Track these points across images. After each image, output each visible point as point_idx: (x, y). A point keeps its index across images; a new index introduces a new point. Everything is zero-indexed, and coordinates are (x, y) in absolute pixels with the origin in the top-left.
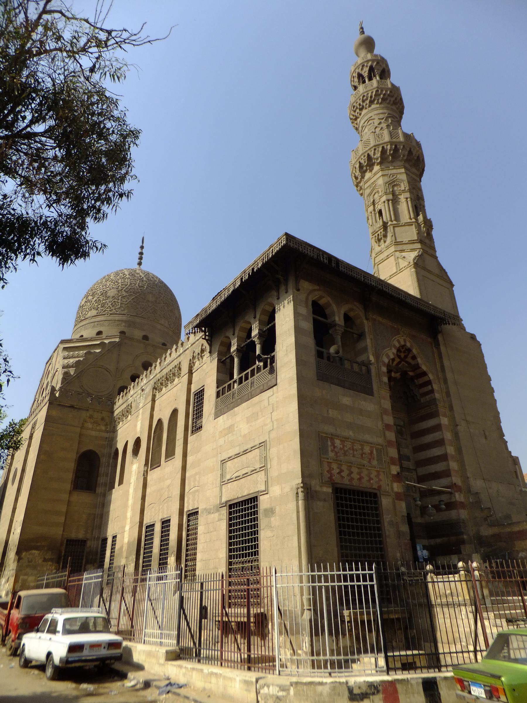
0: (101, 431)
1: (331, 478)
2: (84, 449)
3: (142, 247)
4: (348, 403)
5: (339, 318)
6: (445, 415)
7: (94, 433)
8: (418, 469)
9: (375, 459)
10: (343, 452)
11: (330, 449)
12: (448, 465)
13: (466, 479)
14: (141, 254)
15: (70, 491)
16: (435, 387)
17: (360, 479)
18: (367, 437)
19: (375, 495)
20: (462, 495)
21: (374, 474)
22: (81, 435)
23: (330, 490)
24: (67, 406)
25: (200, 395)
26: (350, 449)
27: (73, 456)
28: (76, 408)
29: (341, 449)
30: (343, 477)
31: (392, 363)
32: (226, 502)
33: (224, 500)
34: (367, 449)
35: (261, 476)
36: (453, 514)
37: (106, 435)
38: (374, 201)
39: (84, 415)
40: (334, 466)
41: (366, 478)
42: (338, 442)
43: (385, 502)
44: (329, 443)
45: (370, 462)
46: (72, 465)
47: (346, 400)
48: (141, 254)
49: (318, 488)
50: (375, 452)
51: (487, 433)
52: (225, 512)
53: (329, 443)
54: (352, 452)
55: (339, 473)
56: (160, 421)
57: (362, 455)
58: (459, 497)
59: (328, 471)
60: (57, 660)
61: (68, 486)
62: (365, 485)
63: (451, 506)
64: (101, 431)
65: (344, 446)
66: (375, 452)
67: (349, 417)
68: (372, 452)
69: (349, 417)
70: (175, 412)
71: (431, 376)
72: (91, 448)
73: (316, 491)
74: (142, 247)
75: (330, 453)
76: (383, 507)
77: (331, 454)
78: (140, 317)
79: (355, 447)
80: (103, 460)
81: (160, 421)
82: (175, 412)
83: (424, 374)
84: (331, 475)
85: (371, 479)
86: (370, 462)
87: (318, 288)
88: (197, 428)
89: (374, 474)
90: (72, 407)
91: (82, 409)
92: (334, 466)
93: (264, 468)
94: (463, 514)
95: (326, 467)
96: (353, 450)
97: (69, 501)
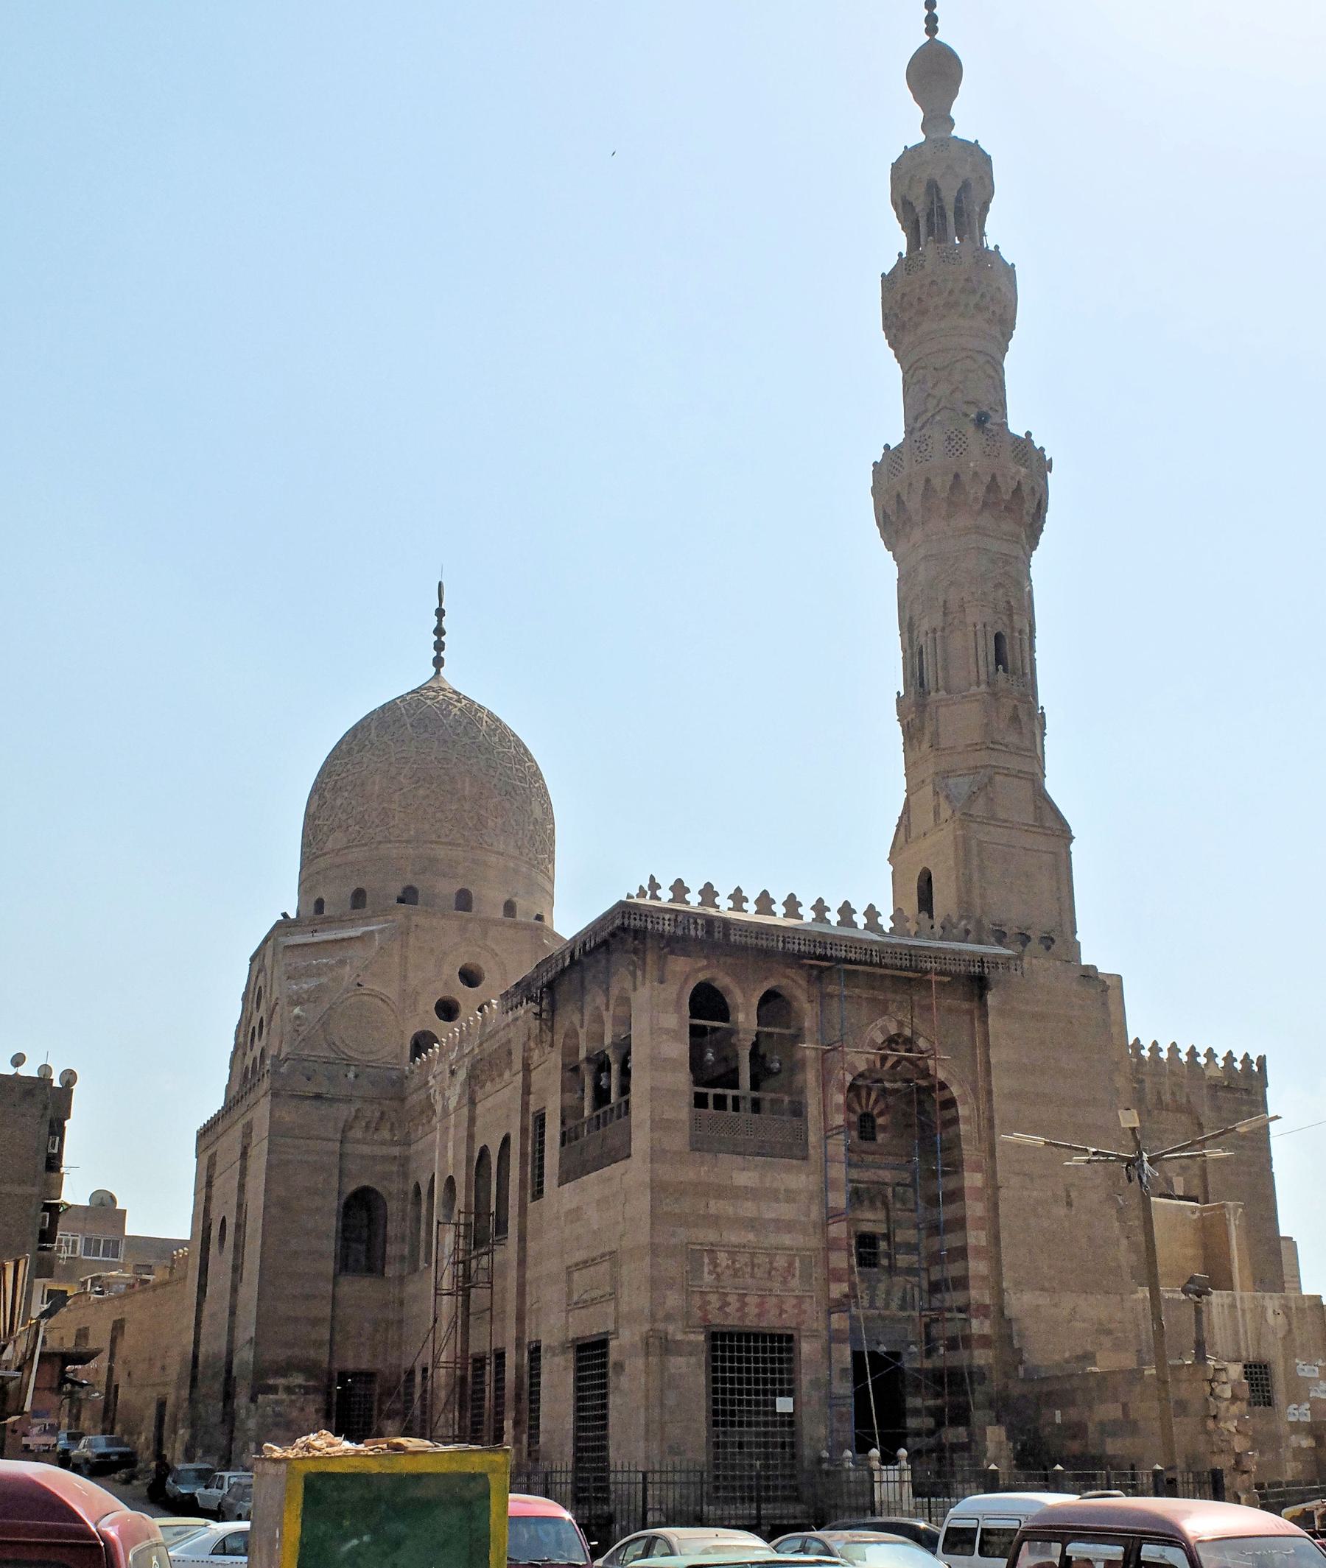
0: (383, 1143)
1: (705, 1319)
2: (351, 1187)
3: (440, 613)
4: (750, 1184)
5: (747, 1015)
6: (978, 1168)
7: (366, 1150)
8: (932, 1269)
9: (797, 1273)
10: (731, 1272)
11: (706, 1270)
12: (967, 1269)
13: (999, 1293)
14: (439, 631)
15: (335, 1276)
16: (963, 1111)
17: (759, 1315)
18: (787, 1240)
19: (790, 1338)
20: (987, 1323)
21: (789, 1304)
22: (342, 1156)
23: (702, 1338)
24: (308, 1098)
25: (540, 1120)
26: (746, 1265)
27: (333, 1204)
28: (326, 1099)
29: (728, 1267)
30: (727, 1314)
31: (883, 1065)
32: (573, 1341)
33: (571, 1335)
34: (781, 1262)
35: (610, 1308)
36: (960, 1359)
37: (396, 1151)
38: (911, 618)
39: (345, 1111)
40: (713, 1298)
41: (775, 1311)
42: (723, 1258)
43: (807, 1348)
44: (706, 1260)
45: (785, 1282)
46: (331, 1224)
47: (744, 1178)
48: (439, 631)
49: (679, 1337)
50: (797, 1264)
51: (1074, 1194)
52: (571, 1356)
53: (706, 1260)
54: (749, 1270)
55: (720, 1308)
56: (484, 1151)
57: (770, 1273)
58: (979, 1326)
59: (700, 1308)
60: (293, 915)
61: (329, 1266)
62: (771, 1322)
63: (967, 1341)
64: (383, 1143)
65: (733, 1263)
66: (797, 1264)
67: (748, 1209)
68: (791, 1265)
69: (748, 1209)
70: (506, 1141)
71: (955, 1090)
72: (366, 1183)
73: (676, 1342)
74: (440, 613)
75: (706, 1275)
76: (803, 1357)
77: (708, 1278)
78: (445, 844)
79: (756, 1261)
80: (393, 1206)
81: (484, 1151)
82: (506, 1141)
83: (943, 1086)
84: (706, 1313)
85: (782, 1311)
86: (785, 1282)
87: (705, 962)
88: (538, 1194)
89: (789, 1304)
90: (318, 1097)
91: (339, 1100)
92: (713, 1298)
93: (613, 1296)
94: (982, 1357)
95: (697, 1300)
96: (753, 1266)
97: (334, 1297)
